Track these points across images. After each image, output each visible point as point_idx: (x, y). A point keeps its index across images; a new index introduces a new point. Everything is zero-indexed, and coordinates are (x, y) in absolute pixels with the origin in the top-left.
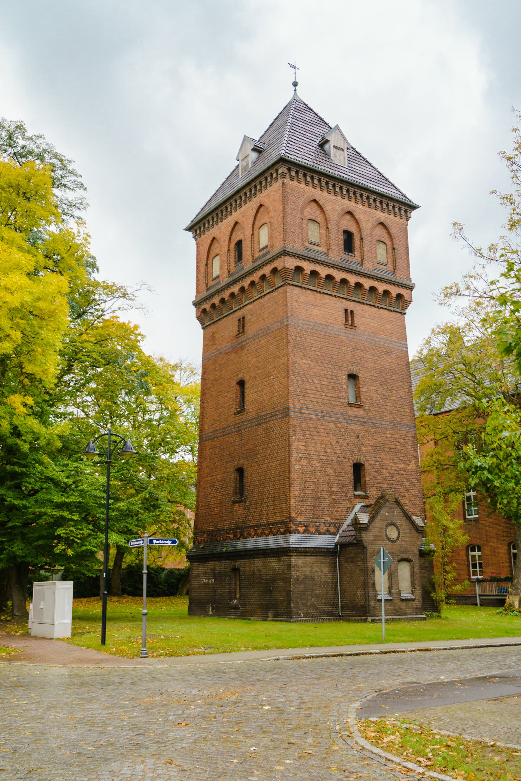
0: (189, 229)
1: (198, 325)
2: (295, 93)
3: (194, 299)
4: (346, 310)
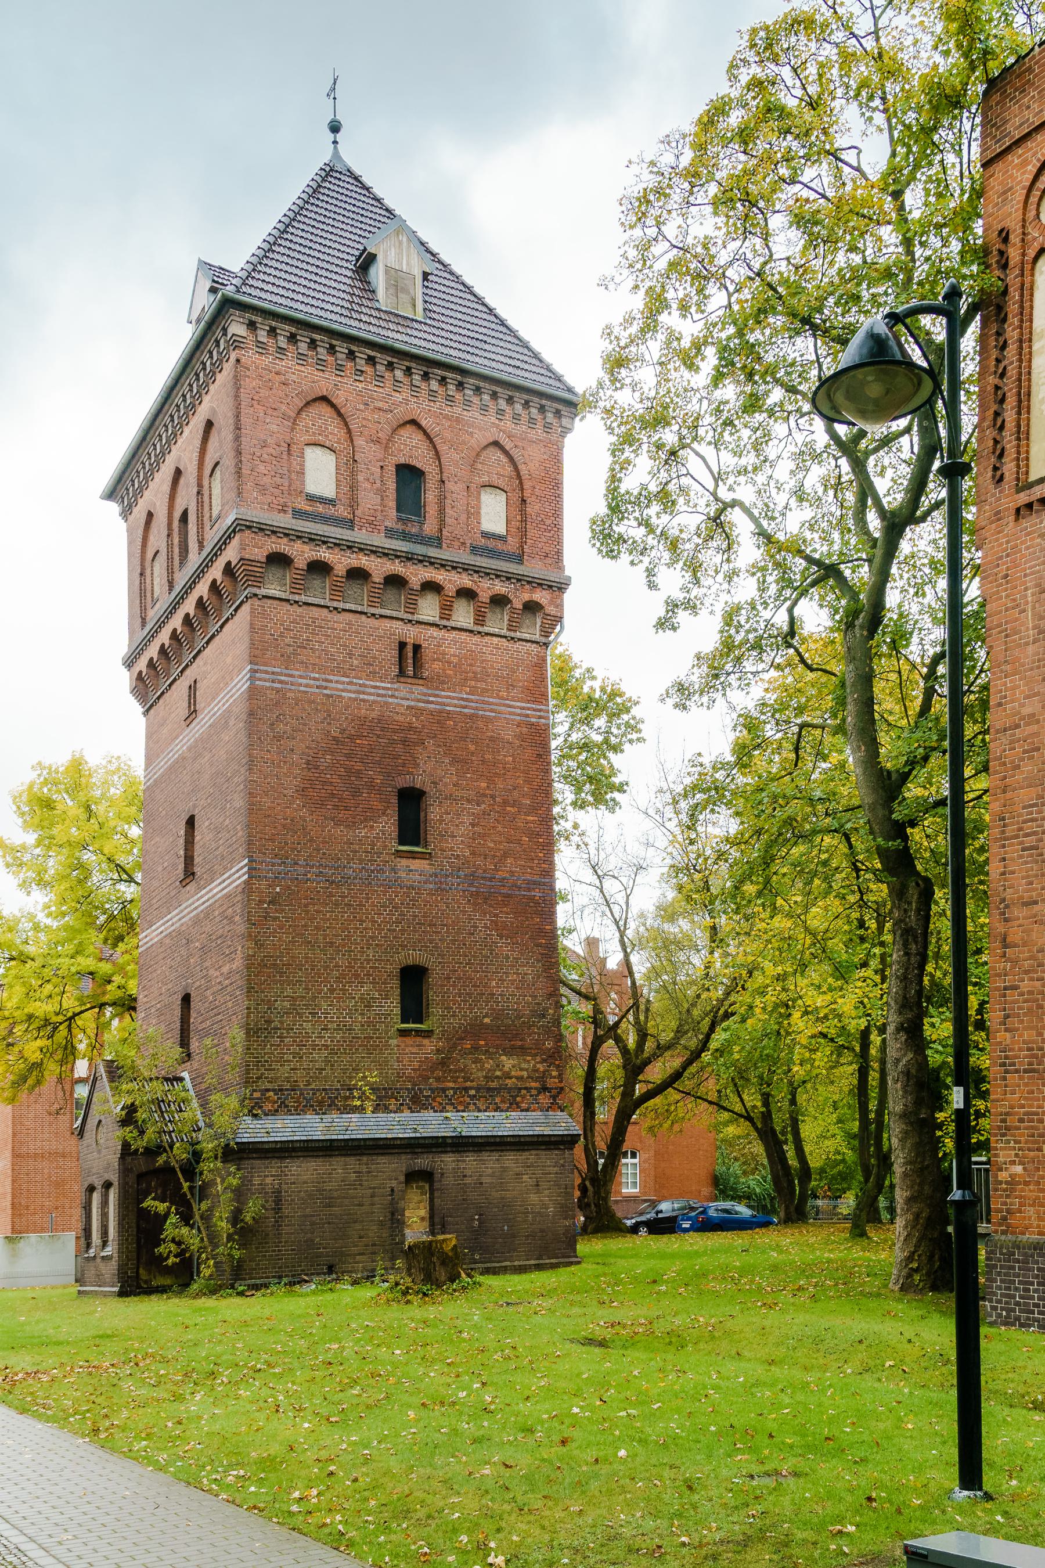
0: (111, 494)
2: (335, 148)
4: (402, 645)
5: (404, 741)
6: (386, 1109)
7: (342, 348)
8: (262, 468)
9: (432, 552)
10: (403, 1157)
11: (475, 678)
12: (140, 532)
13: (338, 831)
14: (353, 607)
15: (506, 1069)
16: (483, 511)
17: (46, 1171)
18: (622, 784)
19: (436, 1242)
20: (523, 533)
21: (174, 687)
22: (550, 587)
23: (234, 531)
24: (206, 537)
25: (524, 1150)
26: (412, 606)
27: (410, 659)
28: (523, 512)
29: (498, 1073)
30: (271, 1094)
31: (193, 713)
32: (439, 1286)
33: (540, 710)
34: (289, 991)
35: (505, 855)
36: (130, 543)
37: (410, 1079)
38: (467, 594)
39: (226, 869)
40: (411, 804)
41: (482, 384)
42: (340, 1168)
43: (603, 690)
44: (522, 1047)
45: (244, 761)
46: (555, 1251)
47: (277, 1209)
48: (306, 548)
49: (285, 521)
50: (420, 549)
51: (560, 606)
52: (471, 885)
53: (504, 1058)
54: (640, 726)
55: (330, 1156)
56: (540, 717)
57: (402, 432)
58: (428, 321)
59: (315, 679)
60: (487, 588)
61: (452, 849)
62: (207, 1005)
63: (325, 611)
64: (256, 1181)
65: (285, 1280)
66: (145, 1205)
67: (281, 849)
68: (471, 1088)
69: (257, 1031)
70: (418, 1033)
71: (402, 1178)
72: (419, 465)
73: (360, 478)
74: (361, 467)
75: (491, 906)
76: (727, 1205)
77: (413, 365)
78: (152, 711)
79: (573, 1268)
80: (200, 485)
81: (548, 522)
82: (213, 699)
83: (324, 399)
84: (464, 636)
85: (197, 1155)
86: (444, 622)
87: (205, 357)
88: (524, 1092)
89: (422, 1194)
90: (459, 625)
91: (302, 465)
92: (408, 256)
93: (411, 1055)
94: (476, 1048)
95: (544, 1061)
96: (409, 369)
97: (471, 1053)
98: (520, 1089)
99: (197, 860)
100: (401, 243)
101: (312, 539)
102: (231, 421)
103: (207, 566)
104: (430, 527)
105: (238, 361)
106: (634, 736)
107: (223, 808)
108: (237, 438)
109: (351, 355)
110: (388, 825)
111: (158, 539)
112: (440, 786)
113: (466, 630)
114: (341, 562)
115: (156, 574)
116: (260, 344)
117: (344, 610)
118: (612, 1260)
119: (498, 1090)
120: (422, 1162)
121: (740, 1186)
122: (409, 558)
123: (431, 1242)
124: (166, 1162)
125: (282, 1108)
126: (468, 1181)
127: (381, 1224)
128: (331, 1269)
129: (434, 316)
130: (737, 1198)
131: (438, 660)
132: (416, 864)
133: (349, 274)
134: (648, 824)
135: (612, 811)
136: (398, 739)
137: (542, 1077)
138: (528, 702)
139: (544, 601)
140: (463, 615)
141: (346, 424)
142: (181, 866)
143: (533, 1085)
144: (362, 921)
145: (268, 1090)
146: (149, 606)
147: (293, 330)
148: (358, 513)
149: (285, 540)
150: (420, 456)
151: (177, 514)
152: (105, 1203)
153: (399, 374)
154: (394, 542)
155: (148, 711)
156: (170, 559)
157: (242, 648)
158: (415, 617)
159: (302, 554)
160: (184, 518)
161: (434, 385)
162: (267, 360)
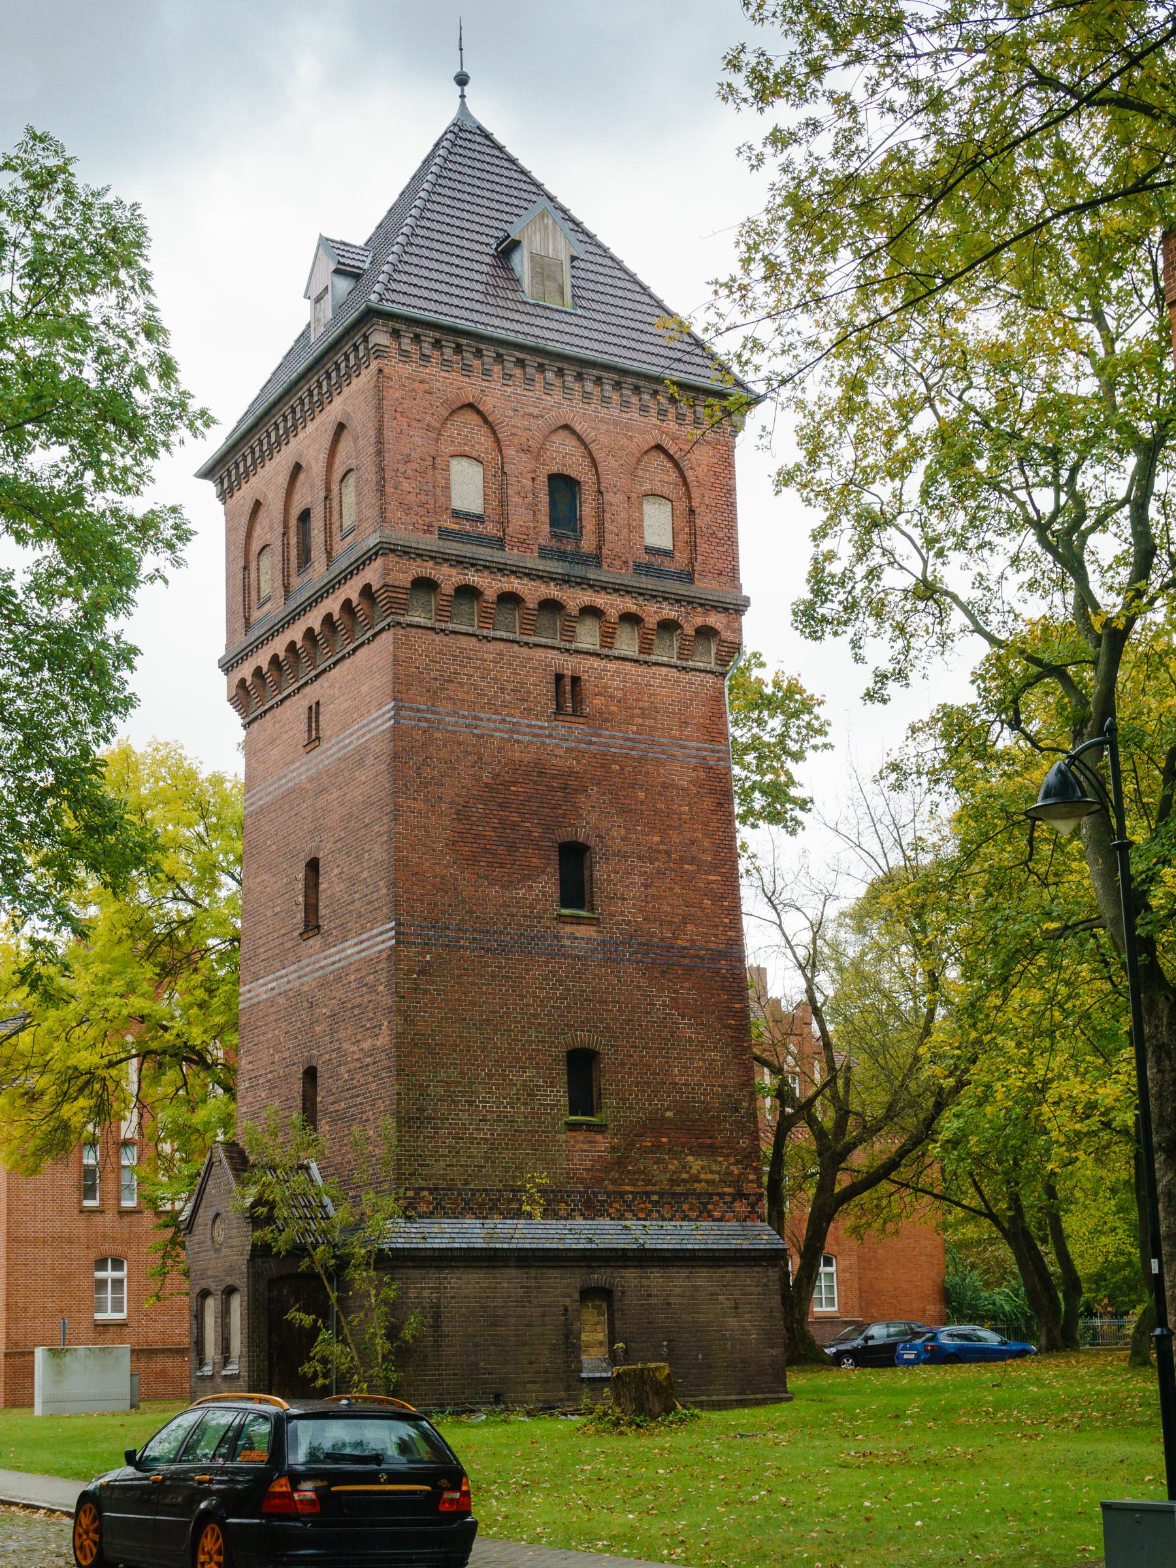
0: (208, 473)
1: (235, 719)
3: (221, 652)
4: (559, 678)
5: (564, 788)
6: (556, 1215)
7: (489, 352)
8: (406, 486)
9: (592, 574)
10: (577, 1271)
11: (643, 716)
12: (244, 520)
13: (493, 892)
14: (504, 635)
15: (694, 1171)
16: (646, 523)
17: (48, 1261)
18: (805, 802)
19: (649, 1370)
20: (694, 547)
21: (287, 703)
22: (726, 609)
23: (376, 554)
24: (335, 547)
25: (718, 1267)
26: (569, 633)
27: (568, 692)
28: (692, 524)
29: (685, 1176)
30: (426, 1193)
31: (314, 740)
32: (654, 1418)
33: (718, 752)
34: (443, 1075)
35: (685, 921)
36: (229, 531)
37: (582, 1180)
38: (631, 619)
39: (364, 929)
40: (574, 860)
41: (641, 383)
42: (509, 1282)
43: (777, 685)
44: (710, 1146)
45: (388, 809)
46: (761, 1386)
47: (436, 1327)
48: (454, 572)
49: (431, 542)
50: (578, 571)
51: (738, 631)
52: (646, 955)
53: (690, 1158)
54: (827, 728)
55: (494, 1267)
56: (719, 759)
57: (554, 438)
58: (579, 312)
59: (464, 717)
60: (654, 613)
61: (622, 913)
62: (340, 1083)
63: (474, 639)
64: (413, 1293)
65: (449, 1409)
66: (289, 1316)
67: (431, 911)
68: (653, 1193)
69: (410, 1120)
70: (590, 1127)
71: (577, 1296)
72: (573, 474)
73: (510, 492)
74: (512, 479)
75: (669, 980)
76: (965, 1328)
77: (566, 366)
78: (255, 725)
79: (784, 1405)
80: (328, 489)
81: (721, 535)
82: (344, 729)
83: (471, 406)
84: (629, 666)
85: (343, 1262)
86: (606, 651)
87: (340, 358)
88: (715, 1198)
89: (599, 1314)
90: (623, 653)
91: (448, 479)
92: (555, 240)
93: (585, 1152)
94: (658, 1147)
95: (737, 1162)
96: (561, 370)
97: (651, 1152)
98: (711, 1195)
99: (322, 911)
100: (546, 227)
101: (459, 562)
102: (372, 433)
103: (339, 582)
104: (588, 544)
105: (380, 371)
106: (819, 740)
107: (359, 857)
108: (379, 453)
109: (499, 358)
110: (548, 885)
111: (268, 530)
112: (606, 840)
113: (631, 660)
114: (491, 585)
115: (263, 570)
116: (404, 353)
117: (494, 639)
118: (830, 1397)
119: (686, 1195)
120: (600, 1277)
121: (982, 1303)
122: (565, 580)
123: (642, 1370)
124: (310, 1268)
125: (438, 1210)
126: (653, 1301)
127: (554, 1347)
128: (498, 1398)
129: (584, 303)
130: (977, 1317)
131: (599, 694)
132: (582, 931)
133: (488, 259)
134: (839, 844)
135: (793, 833)
136: (558, 787)
137: (737, 1182)
138: (705, 741)
139: (719, 626)
140: (627, 643)
141: (494, 433)
142: (300, 916)
143: (727, 1190)
144: (522, 996)
145: (422, 1189)
146: (254, 606)
147: (438, 335)
148: (509, 531)
149: (431, 564)
150: (573, 464)
151: (295, 512)
152: (225, 1312)
153: (550, 375)
154: (549, 562)
155: (249, 723)
156: (286, 560)
157: (382, 680)
158: (573, 646)
159: (449, 577)
160: (305, 516)
161: (589, 386)
162: (409, 369)
